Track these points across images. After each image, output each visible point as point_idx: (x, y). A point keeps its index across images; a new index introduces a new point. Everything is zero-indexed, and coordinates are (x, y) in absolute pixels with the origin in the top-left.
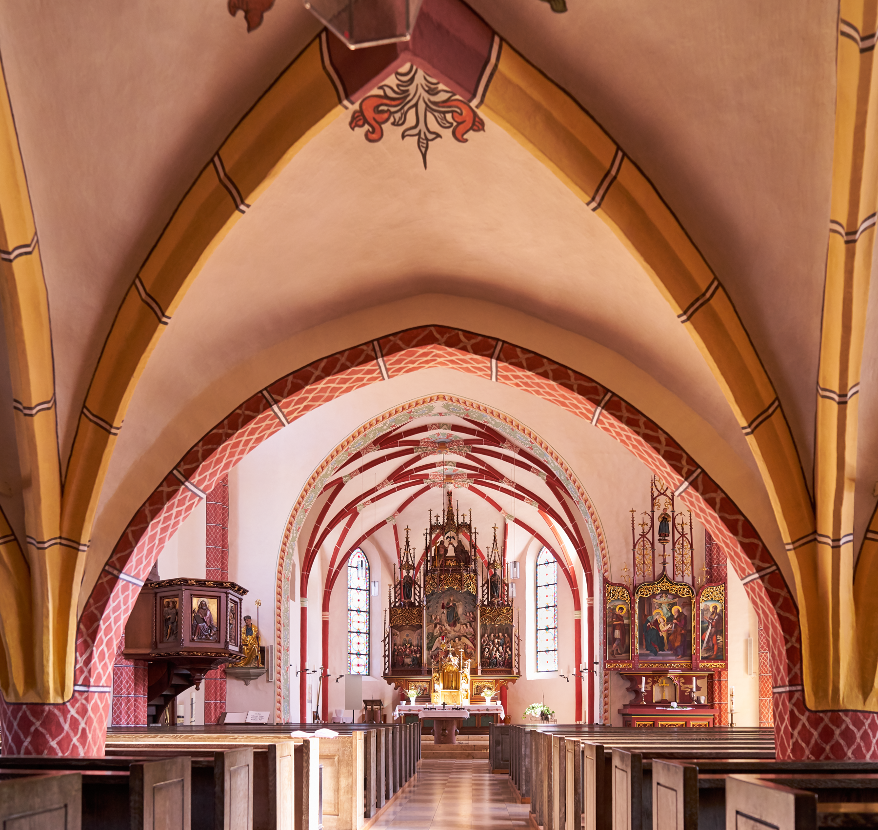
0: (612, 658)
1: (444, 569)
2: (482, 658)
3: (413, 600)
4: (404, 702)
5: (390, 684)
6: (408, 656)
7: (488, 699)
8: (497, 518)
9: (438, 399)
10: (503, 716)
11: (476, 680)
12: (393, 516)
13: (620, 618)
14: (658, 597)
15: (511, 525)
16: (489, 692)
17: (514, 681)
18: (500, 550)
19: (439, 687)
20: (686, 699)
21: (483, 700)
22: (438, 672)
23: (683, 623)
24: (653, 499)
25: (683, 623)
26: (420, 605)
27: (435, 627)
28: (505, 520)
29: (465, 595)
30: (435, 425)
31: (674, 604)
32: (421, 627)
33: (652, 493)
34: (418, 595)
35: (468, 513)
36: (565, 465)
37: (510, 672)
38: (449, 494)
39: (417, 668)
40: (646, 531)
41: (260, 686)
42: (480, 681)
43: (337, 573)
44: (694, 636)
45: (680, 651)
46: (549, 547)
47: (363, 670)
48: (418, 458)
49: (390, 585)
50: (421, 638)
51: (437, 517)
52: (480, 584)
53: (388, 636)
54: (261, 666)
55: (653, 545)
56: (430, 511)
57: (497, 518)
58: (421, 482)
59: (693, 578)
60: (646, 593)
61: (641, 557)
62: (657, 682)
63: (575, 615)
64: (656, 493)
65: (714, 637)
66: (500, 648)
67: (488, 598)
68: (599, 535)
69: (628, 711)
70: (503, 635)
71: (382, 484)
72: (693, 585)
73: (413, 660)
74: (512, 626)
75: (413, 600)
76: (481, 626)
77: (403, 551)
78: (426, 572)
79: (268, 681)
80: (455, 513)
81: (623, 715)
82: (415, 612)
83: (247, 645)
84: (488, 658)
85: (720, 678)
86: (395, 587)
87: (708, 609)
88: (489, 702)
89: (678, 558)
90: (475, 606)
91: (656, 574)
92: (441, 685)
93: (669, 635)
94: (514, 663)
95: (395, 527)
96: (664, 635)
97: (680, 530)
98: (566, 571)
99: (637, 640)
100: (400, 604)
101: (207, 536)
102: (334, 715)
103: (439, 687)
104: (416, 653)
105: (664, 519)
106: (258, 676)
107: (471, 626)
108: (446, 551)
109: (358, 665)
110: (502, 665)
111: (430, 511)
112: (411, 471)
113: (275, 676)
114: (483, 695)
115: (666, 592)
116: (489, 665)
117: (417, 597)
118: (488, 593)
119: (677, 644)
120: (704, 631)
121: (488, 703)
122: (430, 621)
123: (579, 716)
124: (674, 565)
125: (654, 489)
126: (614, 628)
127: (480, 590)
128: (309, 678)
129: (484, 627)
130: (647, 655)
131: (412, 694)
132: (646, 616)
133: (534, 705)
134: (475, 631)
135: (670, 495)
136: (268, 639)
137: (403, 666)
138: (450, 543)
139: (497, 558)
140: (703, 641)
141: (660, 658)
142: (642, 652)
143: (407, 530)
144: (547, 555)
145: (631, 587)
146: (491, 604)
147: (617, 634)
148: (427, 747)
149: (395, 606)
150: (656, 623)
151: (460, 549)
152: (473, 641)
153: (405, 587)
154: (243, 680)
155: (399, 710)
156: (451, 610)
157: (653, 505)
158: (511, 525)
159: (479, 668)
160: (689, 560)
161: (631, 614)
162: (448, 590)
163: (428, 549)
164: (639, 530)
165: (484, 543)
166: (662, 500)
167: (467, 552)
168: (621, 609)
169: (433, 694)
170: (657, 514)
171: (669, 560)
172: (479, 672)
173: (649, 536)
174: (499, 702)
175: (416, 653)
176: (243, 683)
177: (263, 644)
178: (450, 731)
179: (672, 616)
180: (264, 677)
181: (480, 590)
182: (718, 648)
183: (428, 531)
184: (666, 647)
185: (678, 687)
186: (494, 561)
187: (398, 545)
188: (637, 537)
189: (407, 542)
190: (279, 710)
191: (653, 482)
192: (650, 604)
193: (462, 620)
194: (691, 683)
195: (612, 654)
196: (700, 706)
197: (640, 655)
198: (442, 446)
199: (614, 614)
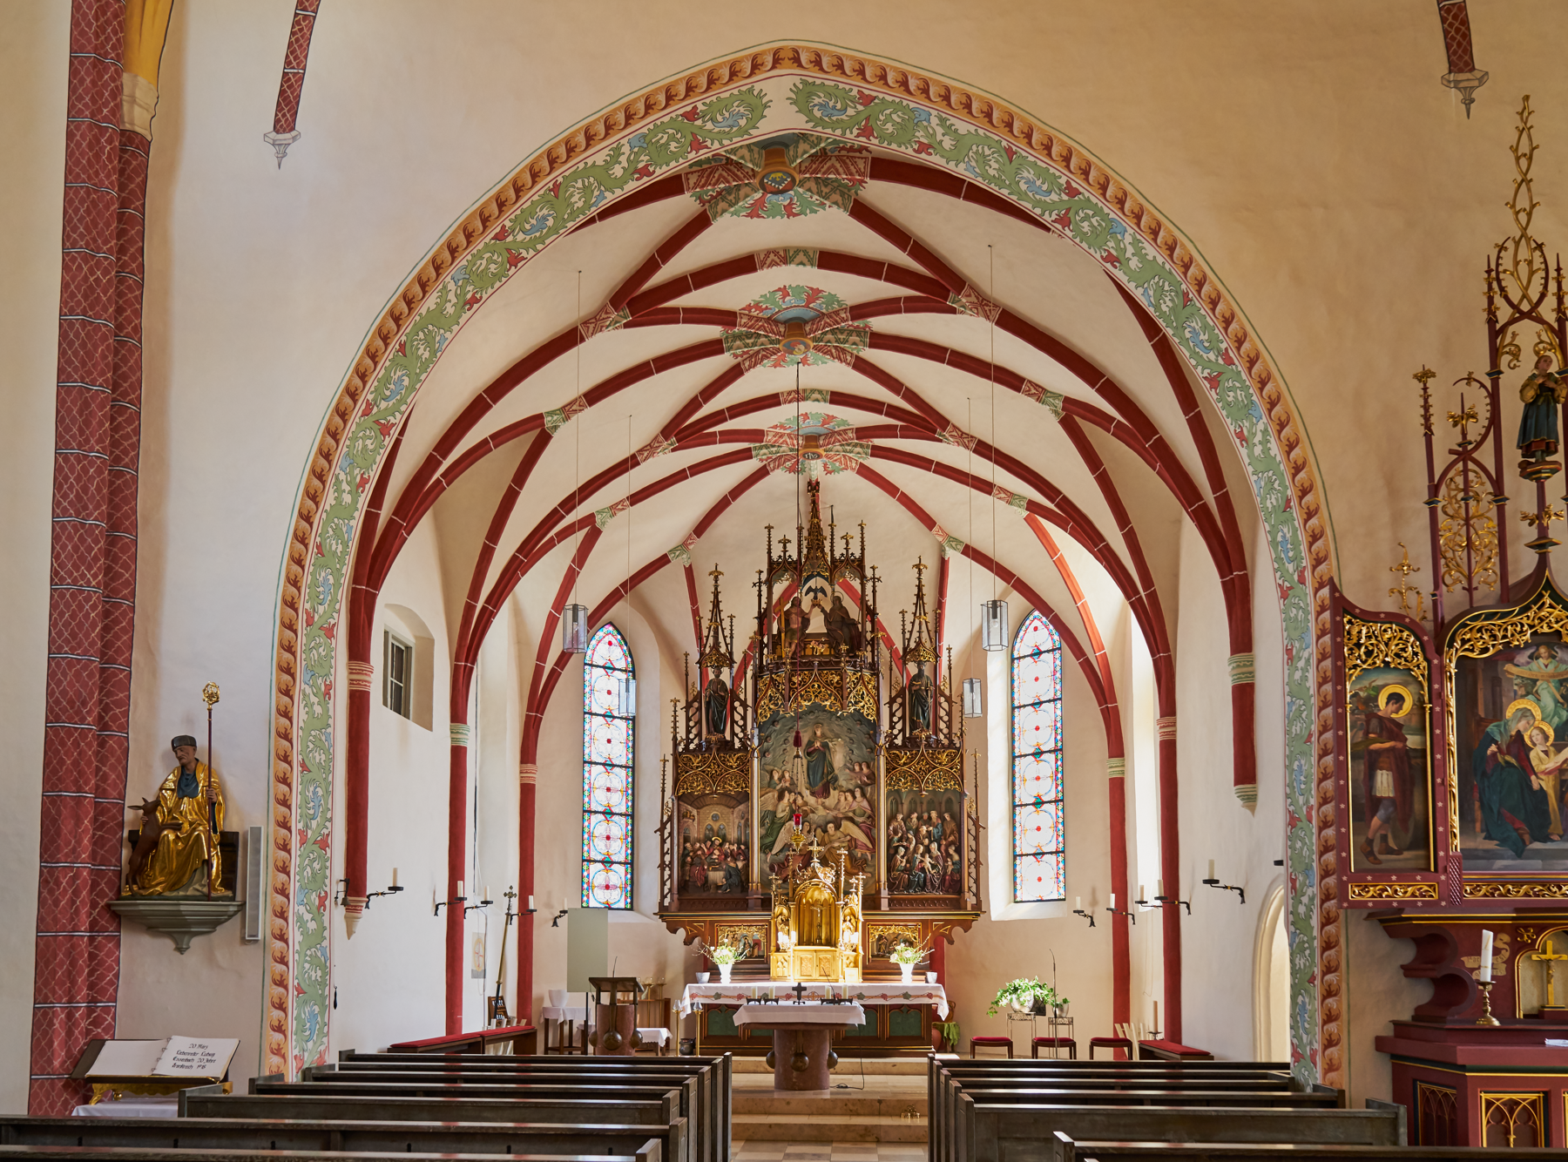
0: (1368, 865)
1: (801, 663)
2: (889, 870)
3: (728, 737)
4: (707, 975)
5: (674, 931)
6: (715, 866)
7: (907, 969)
8: (923, 544)
9: (777, 62)
10: (943, 1011)
11: (876, 923)
12: (684, 546)
13: (1393, 730)
14: (1522, 658)
15: (955, 559)
16: (910, 953)
17: (966, 926)
18: (930, 617)
19: (787, 938)
21: (896, 971)
22: (786, 903)
24: (1495, 333)
26: (744, 747)
27: (781, 797)
28: (942, 550)
29: (850, 723)
30: (775, 252)
32: (746, 797)
34: (743, 725)
35: (856, 533)
36: (1186, 247)
37: (958, 904)
38: (813, 487)
39: (739, 895)
40: (1473, 436)
41: (220, 956)
42: (886, 923)
43: (554, 676)
46: (1046, 609)
47: (617, 898)
48: (734, 373)
49: (675, 702)
50: (748, 824)
51: (785, 542)
52: (885, 698)
53: (670, 819)
54: (222, 892)
55: (1498, 483)
56: (769, 528)
57: (923, 544)
58: (745, 455)
60: (1479, 644)
61: (1458, 525)
62: (1531, 946)
63: (1110, 768)
64: (1504, 313)
66: (934, 846)
67: (903, 730)
68: (1297, 469)
69: (1405, 1047)
70: (941, 816)
71: (650, 449)
73: (729, 876)
74: (962, 795)
75: (728, 737)
76: (889, 794)
77: (705, 624)
78: (759, 672)
79: (244, 941)
80: (826, 532)
81: (1393, 1056)
82: (733, 762)
83: (177, 827)
84: (905, 870)
86: (688, 706)
88: (909, 977)
90: (873, 749)
92: (794, 935)
94: (968, 882)
95: (689, 572)
96: (1547, 784)
98: (1087, 666)
99: (1455, 805)
100: (699, 745)
101: (57, 486)
102: (547, 1004)
103: (787, 938)
104: (735, 859)
106: (213, 923)
107: (863, 795)
108: (806, 622)
109: (606, 888)
110: (935, 887)
111: (769, 528)
112: (719, 417)
113: (265, 923)
114: (894, 958)
116: (907, 887)
117: (737, 730)
118: (903, 718)
121: (907, 980)
122: (768, 785)
123: (1122, 1011)
125: (1499, 301)
126: (1372, 763)
127: (885, 711)
128: (472, 924)
129: (895, 796)
130: (1489, 856)
131: (725, 957)
132: (1483, 723)
133: (1017, 982)
134: (874, 806)
135: (1551, 318)
136: (247, 806)
137: (703, 892)
138: (815, 604)
139: (925, 635)
141: (1533, 868)
142: (1471, 845)
143: (716, 574)
144: (1040, 634)
145: (1429, 626)
146: (911, 743)
147: (1384, 783)
148: (754, 1101)
149: (686, 748)
150: (1519, 745)
151: (837, 617)
152: (870, 829)
153: (713, 705)
154: (170, 935)
155: (692, 996)
156: (818, 759)
157: (1495, 353)
158: (955, 559)
159: (885, 893)
161: (1428, 715)
162: (811, 710)
163: (763, 617)
164: (1446, 438)
165: (894, 610)
167: (854, 623)
168: (1396, 699)
169: (774, 957)
170: (1513, 380)
172: (884, 903)
173: (1486, 455)
174: (932, 976)
175: (735, 859)
176: (168, 944)
177: (232, 822)
178: (816, 1059)
180: (232, 926)
181: (885, 711)
183: (764, 577)
186: (919, 643)
187: (696, 613)
189: (716, 603)
190: (279, 1029)
191: (1493, 276)
192: (1496, 683)
193: (842, 782)
195: (1367, 850)
197: (1468, 854)
198: (793, 330)
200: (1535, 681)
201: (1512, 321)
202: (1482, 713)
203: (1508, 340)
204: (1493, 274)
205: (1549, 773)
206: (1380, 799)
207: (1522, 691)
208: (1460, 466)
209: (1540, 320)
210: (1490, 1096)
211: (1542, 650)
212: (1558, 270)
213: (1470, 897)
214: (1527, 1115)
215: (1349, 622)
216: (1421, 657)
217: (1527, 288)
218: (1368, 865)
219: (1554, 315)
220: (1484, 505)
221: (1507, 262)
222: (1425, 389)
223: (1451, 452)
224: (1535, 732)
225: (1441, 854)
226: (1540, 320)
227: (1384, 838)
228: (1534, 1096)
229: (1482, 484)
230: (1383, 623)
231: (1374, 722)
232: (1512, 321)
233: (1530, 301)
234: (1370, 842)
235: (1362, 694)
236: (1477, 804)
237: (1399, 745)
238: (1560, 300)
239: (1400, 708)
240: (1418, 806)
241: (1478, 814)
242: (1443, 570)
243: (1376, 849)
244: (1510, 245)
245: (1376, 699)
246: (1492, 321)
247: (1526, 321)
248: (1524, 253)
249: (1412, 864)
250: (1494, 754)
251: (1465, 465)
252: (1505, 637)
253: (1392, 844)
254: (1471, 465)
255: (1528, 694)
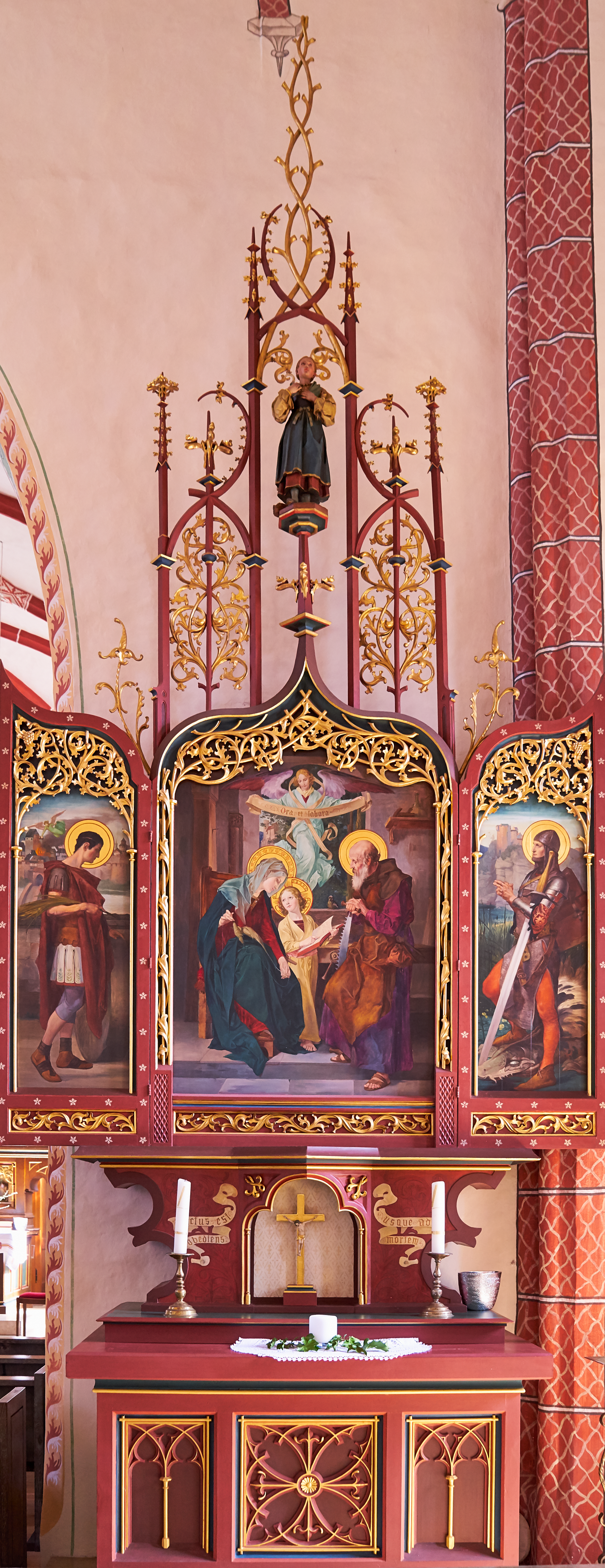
0: (42, 1082)
13: (82, 885)
14: (273, 786)
20: (395, 1290)
23: (394, 914)
24: (258, 330)
25: (393, 914)
31: (348, 823)
33: (254, 303)
40: (222, 472)
44: (443, 977)
45: (377, 1053)
55: (252, 538)
59: (445, 696)
60: (217, 765)
61: (194, 595)
64: (270, 307)
65: (544, 986)
72: (445, 732)
85: (569, 1182)
87: (515, 849)
89: (376, 603)
91: (269, 691)
93: (324, 972)
97: (384, 474)
105: (304, 410)
115: (313, 761)
119: (365, 1017)
120: (493, 952)
124: (354, 638)
126: (52, 933)
130: (215, 1071)
132: (211, 879)
135: (337, 318)
140: (488, 1004)
141: (277, 1088)
142: (191, 1055)
147: (69, 963)
150: (263, 913)
157: (256, 358)
160: (426, 614)
161: (137, 871)
164: (187, 470)
166: (300, 337)
168: (91, 840)
170: (275, 387)
171: (331, 609)
173: (237, 498)
179: (341, 878)
182: (563, 1039)
184: (311, 1030)
185: (366, 1230)
188: (180, 502)
191: (259, 256)
192: (234, 822)
194: (426, 1211)
196: (467, 1329)
199: (52, 865)
200: (289, 821)
201: (281, 318)
202: (213, 865)
203: (275, 343)
204: (259, 254)
205: (305, 953)
206: (62, 987)
207: (270, 835)
208: (203, 511)
209: (319, 318)
210: (135, 1422)
211: (301, 776)
212: (348, 254)
213: (187, 1132)
214: (188, 1449)
215: (24, 726)
216: (125, 779)
217: (302, 278)
218: (42, 1082)
219: (341, 314)
220: (417, 575)
221: (277, 238)
222: (163, 405)
223: (192, 493)
224: (287, 894)
225: (143, 1068)
226: (319, 318)
227: (66, 1044)
228: (198, 1422)
229: (231, 538)
230: (73, 729)
231: (58, 873)
232: (281, 318)
233: (307, 292)
234: (45, 1050)
235: (40, 832)
236: (202, 997)
237: (92, 908)
238: (349, 290)
239: (96, 854)
240: (115, 998)
241: (203, 1010)
242: (173, 658)
243: (53, 1060)
244: (282, 215)
245: (61, 840)
246: (254, 315)
247: (301, 318)
248: (300, 227)
249: (104, 1083)
250: (228, 925)
251: (210, 512)
252: (247, 755)
253: (76, 1052)
254: (217, 512)
255: (278, 838)
